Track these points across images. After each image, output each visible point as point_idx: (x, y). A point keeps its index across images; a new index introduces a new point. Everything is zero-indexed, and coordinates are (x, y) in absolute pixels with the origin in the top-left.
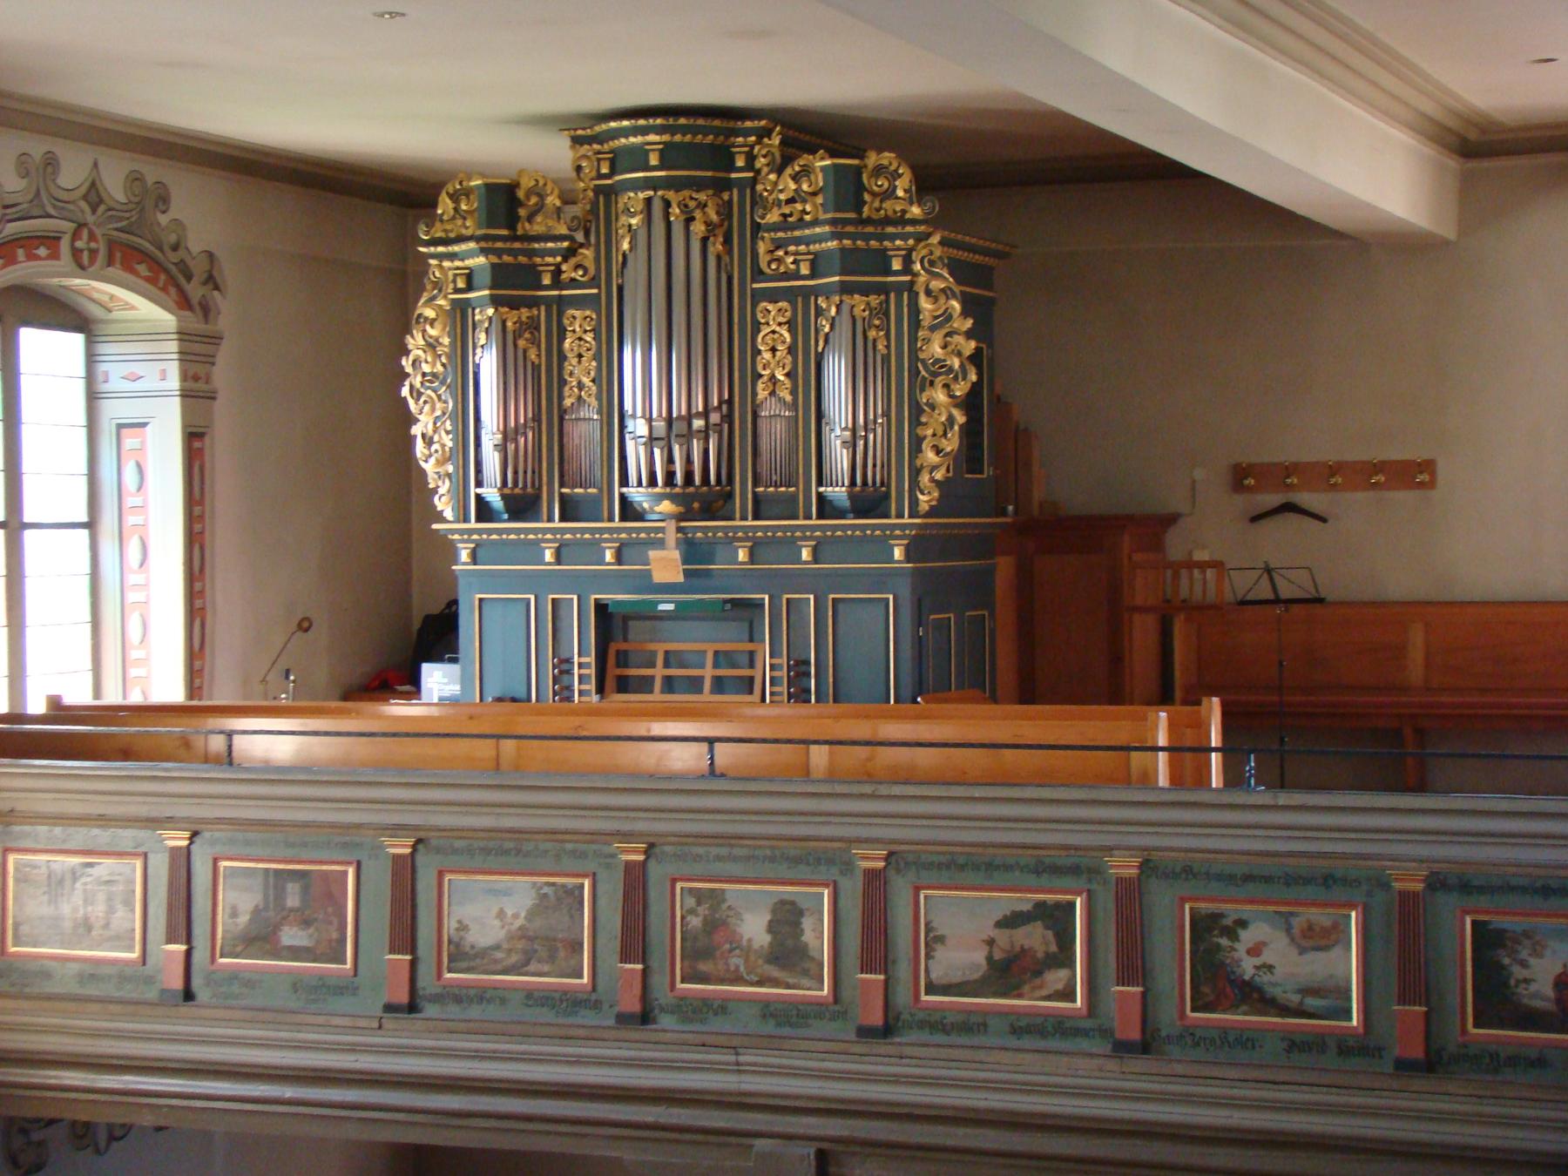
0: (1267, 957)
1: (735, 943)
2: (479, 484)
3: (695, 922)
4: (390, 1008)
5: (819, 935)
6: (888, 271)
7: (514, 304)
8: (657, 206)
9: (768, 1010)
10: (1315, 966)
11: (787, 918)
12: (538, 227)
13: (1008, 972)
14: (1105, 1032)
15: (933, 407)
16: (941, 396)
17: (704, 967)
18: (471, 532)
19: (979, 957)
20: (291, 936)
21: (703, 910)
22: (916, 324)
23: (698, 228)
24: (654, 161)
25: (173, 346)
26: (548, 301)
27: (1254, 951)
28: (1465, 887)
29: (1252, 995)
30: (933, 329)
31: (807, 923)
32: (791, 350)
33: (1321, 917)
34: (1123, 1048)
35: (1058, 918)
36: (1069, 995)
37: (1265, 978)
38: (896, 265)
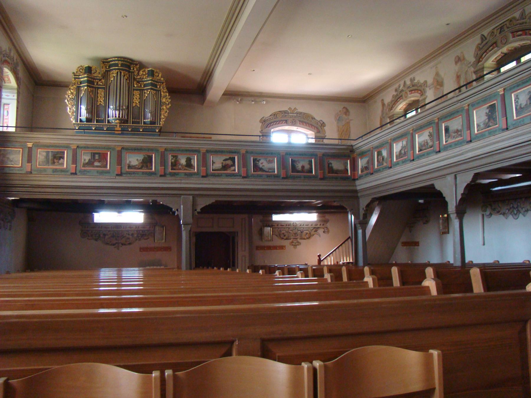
0: (264, 164)
1: (180, 164)
2: (80, 116)
3: (173, 161)
4: (117, 175)
5: (195, 163)
6: (157, 87)
7: (90, 87)
8: (119, 73)
9: (186, 174)
10: (270, 166)
11: (189, 160)
12: (95, 75)
13: (225, 167)
14: (240, 176)
15: (163, 109)
16: (164, 108)
17: (174, 168)
18: (79, 124)
19: (221, 165)
20: (96, 164)
21: (174, 159)
22: (161, 96)
23: (126, 77)
24: (120, 65)
25: (16, 91)
26: (95, 88)
27: (262, 163)
28: (290, 154)
29: (261, 170)
30: (164, 97)
31: (192, 161)
32: (140, 99)
33: (271, 159)
34: (244, 177)
35: (233, 160)
36: (235, 170)
37: (263, 167)
38: (158, 87)
